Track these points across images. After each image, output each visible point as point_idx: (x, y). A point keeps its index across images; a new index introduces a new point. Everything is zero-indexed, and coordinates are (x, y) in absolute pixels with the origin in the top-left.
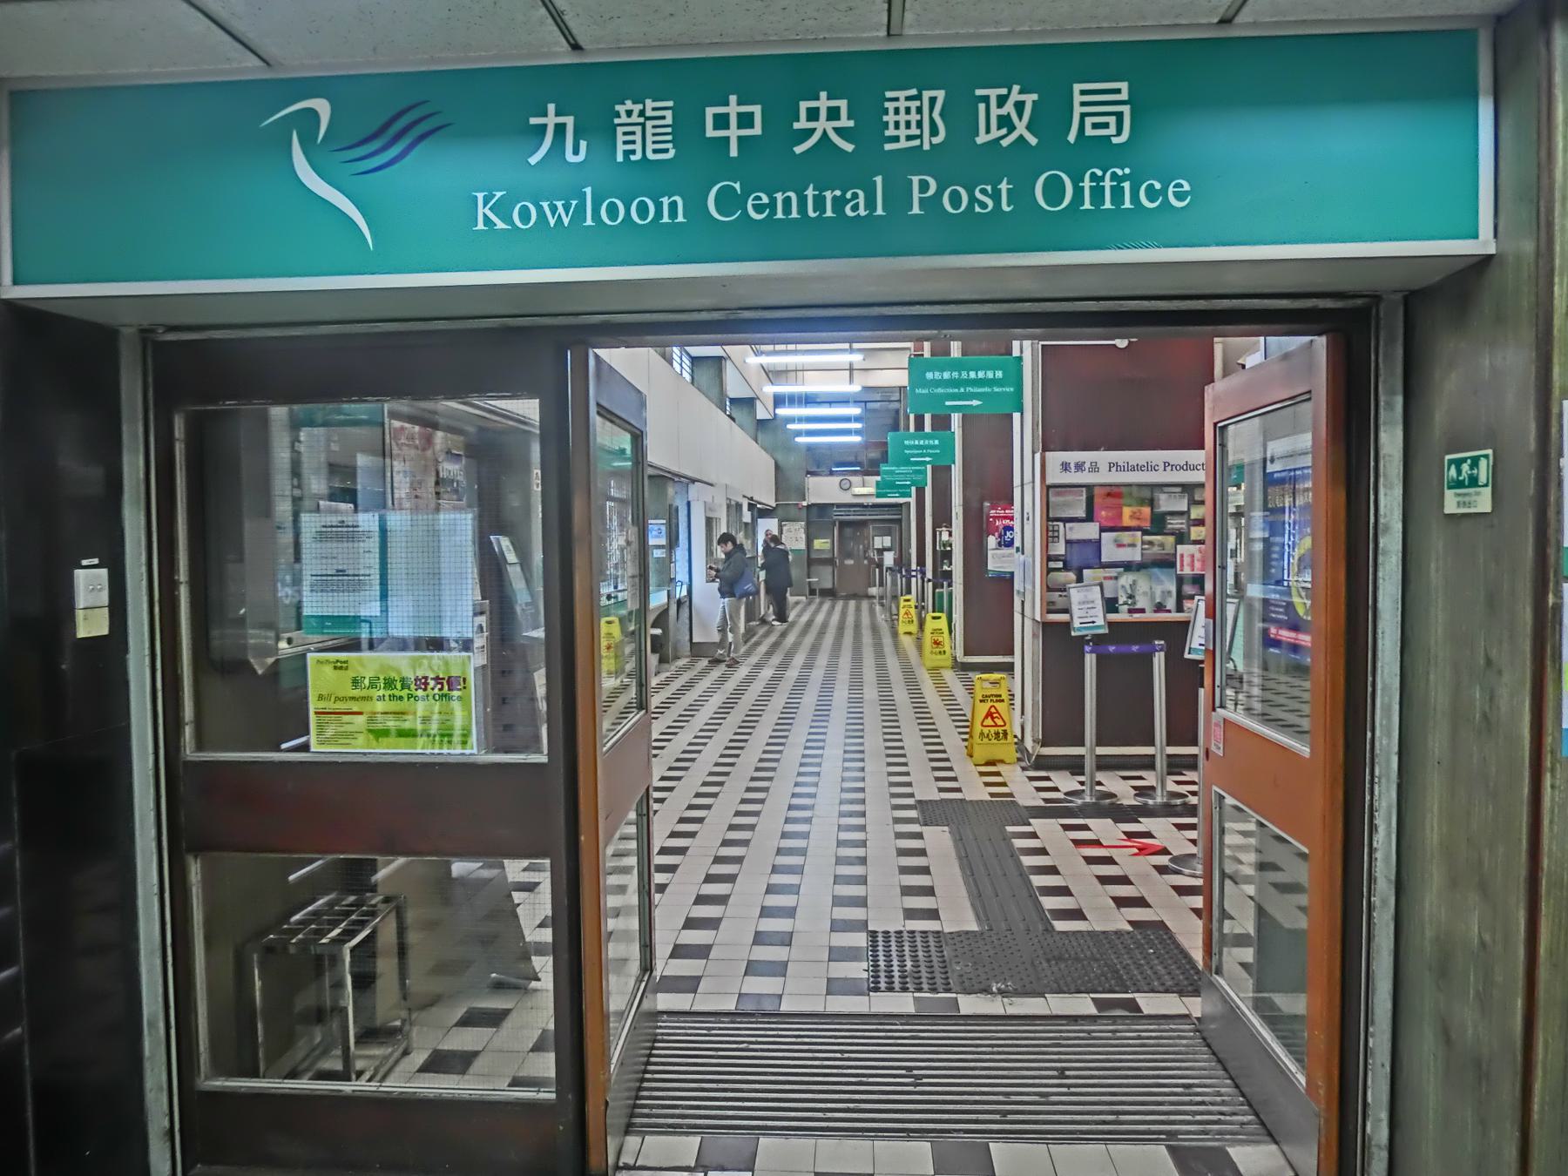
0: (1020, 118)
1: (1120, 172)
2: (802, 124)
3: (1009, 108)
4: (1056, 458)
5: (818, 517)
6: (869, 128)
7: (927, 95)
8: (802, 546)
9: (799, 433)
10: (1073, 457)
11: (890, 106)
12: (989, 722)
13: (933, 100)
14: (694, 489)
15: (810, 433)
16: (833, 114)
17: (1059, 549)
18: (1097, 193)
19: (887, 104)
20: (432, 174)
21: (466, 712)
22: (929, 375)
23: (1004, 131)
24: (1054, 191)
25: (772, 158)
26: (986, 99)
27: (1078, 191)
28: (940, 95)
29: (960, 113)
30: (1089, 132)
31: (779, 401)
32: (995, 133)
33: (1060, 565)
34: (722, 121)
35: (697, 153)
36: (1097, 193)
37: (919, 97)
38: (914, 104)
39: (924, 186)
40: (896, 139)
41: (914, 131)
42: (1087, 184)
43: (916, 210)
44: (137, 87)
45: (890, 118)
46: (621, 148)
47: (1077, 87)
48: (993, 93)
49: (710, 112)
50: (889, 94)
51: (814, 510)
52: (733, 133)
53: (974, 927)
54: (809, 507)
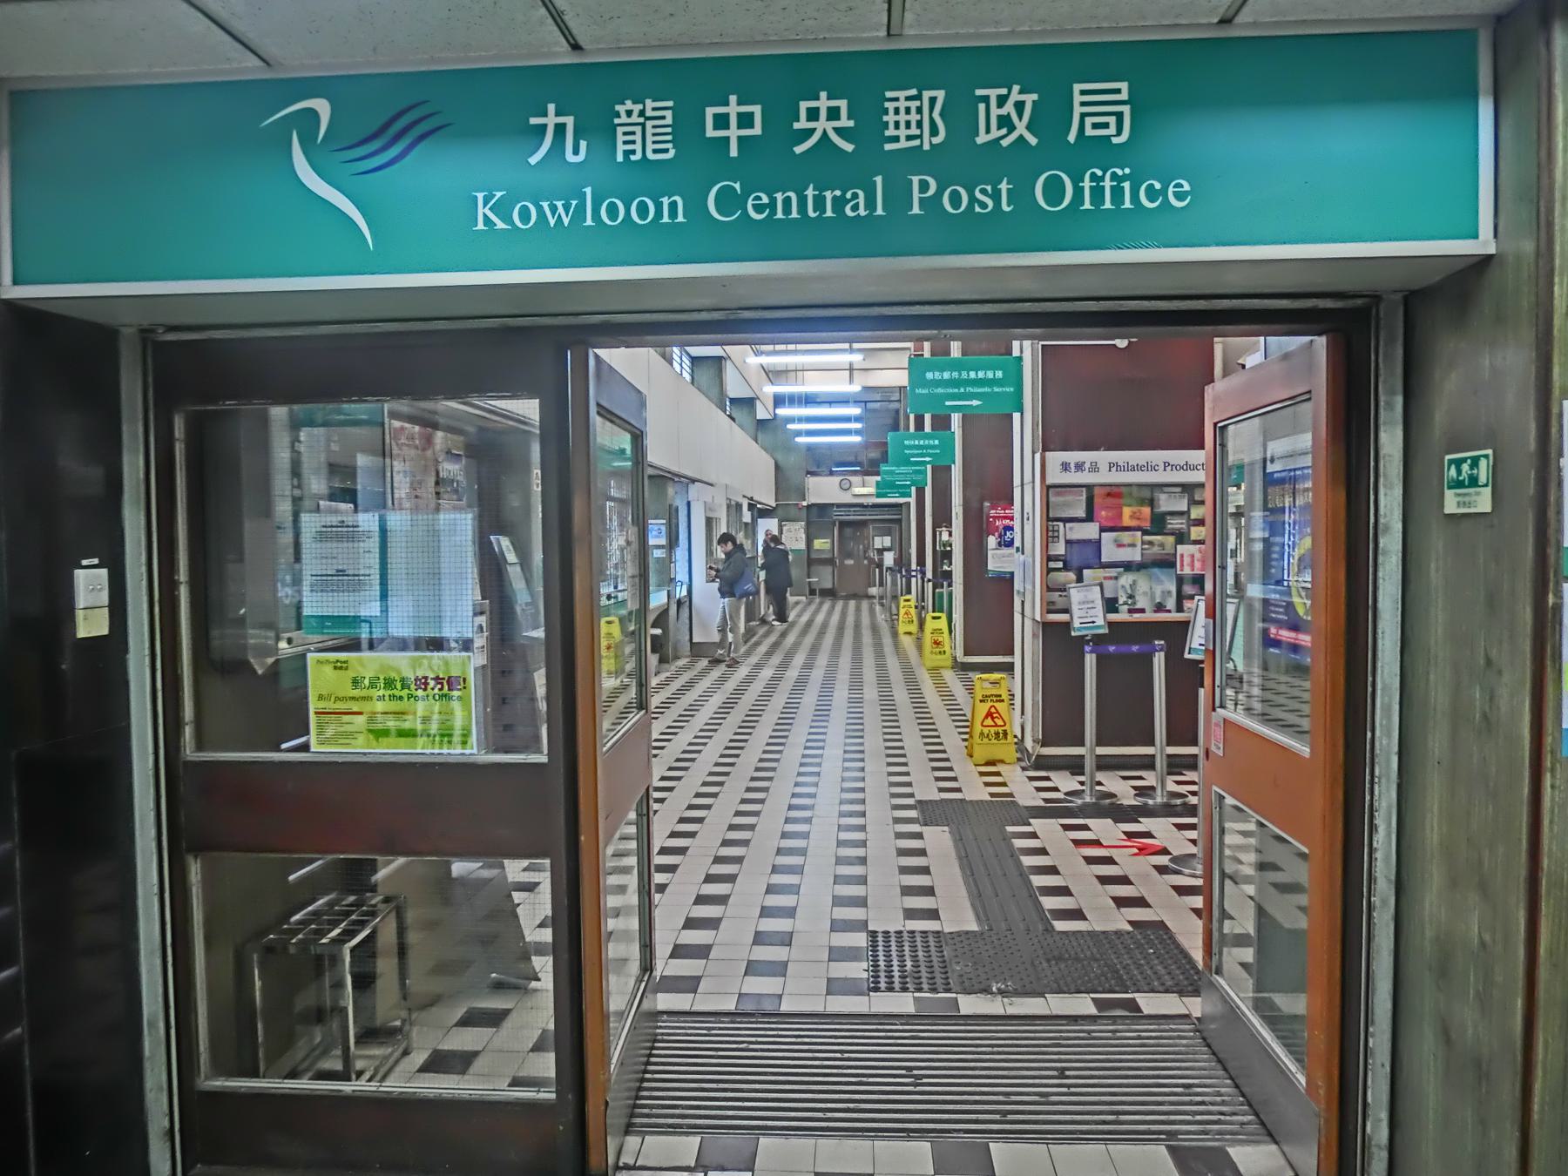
0: (1020, 118)
1: (1120, 172)
2: (802, 124)
3: (1009, 108)
4: (1056, 458)
5: (818, 517)
6: (869, 128)
7: (927, 95)
8: (802, 546)
9: (799, 433)
10: (1073, 457)
11: (890, 106)
12: (989, 722)
13: (933, 100)
14: (694, 489)
15: (810, 433)
16: (833, 114)
17: (1059, 549)
18: (1097, 193)
19: (887, 104)
20: (432, 174)
21: (466, 712)
22: (929, 375)
23: (1004, 131)
24: (1054, 191)
25: (772, 158)
26: (986, 99)
27: (1078, 191)
28: (940, 95)
29: (960, 113)
30: (1089, 132)
31: (779, 401)
32: (995, 133)
33: (1060, 565)
34: (722, 121)
35: (697, 153)
36: (1097, 193)
37: (919, 97)
38: (914, 104)
39: (924, 186)
40: (896, 139)
41: (914, 131)
42: (1087, 184)
43: (916, 210)
44: (137, 87)
45: (890, 118)
46: (621, 148)
47: (1077, 87)
48: (993, 93)
49: (710, 112)
50: (889, 94)
51: (814, 510)
52: (733, 133)
53: (974, 927)
54: (809, 507)
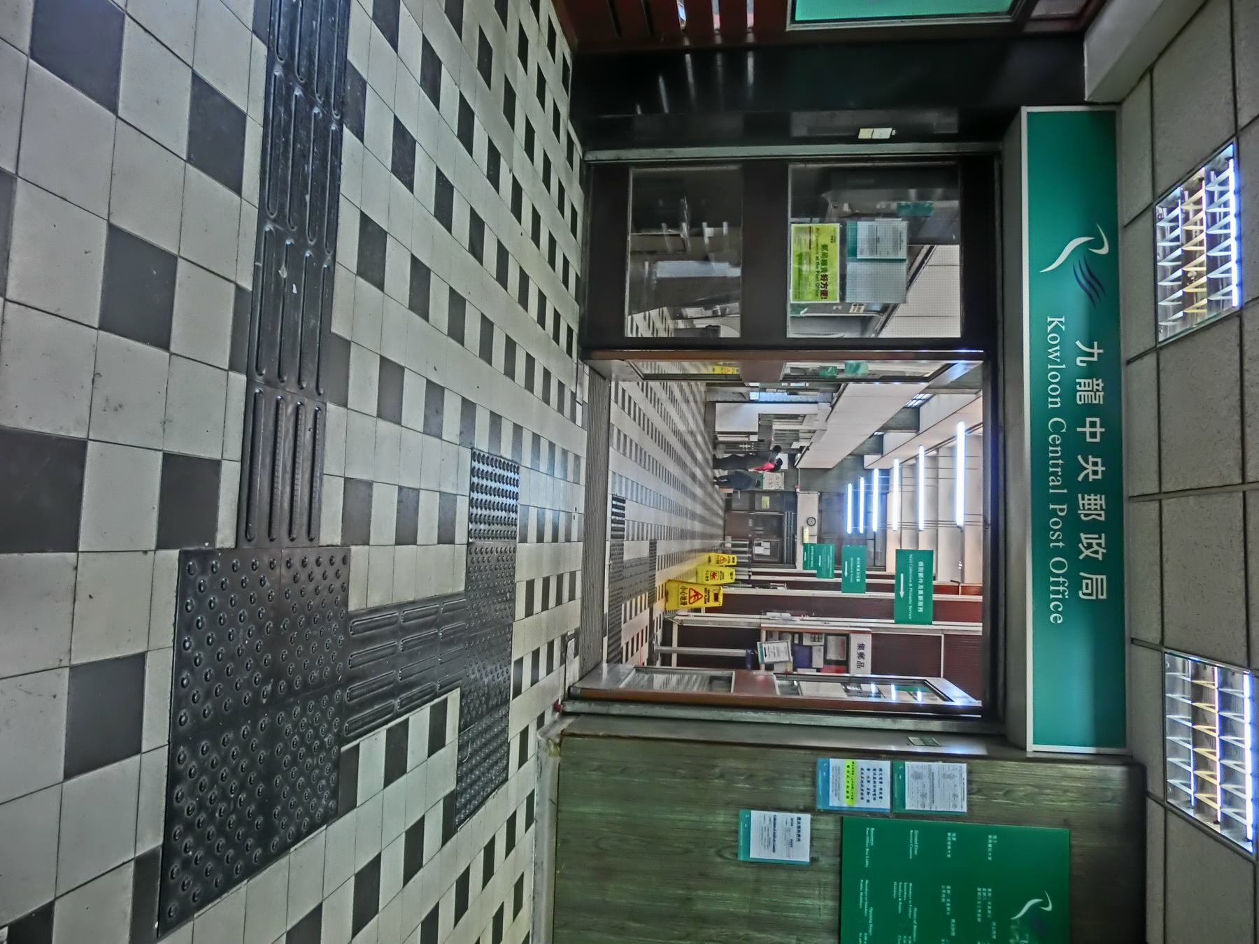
2: (1091, 459)
3: (1096, 548)
4: (868, 641)
5: (787, 500)
6: (1090, 487)
7: (1103, 513)
8: (766, 487)
9: (856, 487)
10: (868, 652)
12: (693, 593)
14: (826, 406)
15: (856, 495)
16: (1095, 473)
17: (806, 642)
18: (1057, 584)
20: (1074, 294)
21: (810, 298)
22: (921, 564)
24: (1059, 565)
25: (1075, 446)
26: (1100, 538)
27: (1058, 576)
28: (1102, 519)
29: (1093, 527)
30: (1084, 582)
31: (886, 473)
32: (1085, 541)
33: (796, 642)
34: (1093, 425)
35: (1079, 413)
36: (1057, 584)
39: (1062, 510)
42: (1061, 579)
44: (1115, 172)
46: (1082, 381)
47: (1104, 577)
48: (1103, 541)
49: (1098, 420)
51: (791, 499)
52: (1088, 430)
53: (626, 558)
54: (795, 494)
